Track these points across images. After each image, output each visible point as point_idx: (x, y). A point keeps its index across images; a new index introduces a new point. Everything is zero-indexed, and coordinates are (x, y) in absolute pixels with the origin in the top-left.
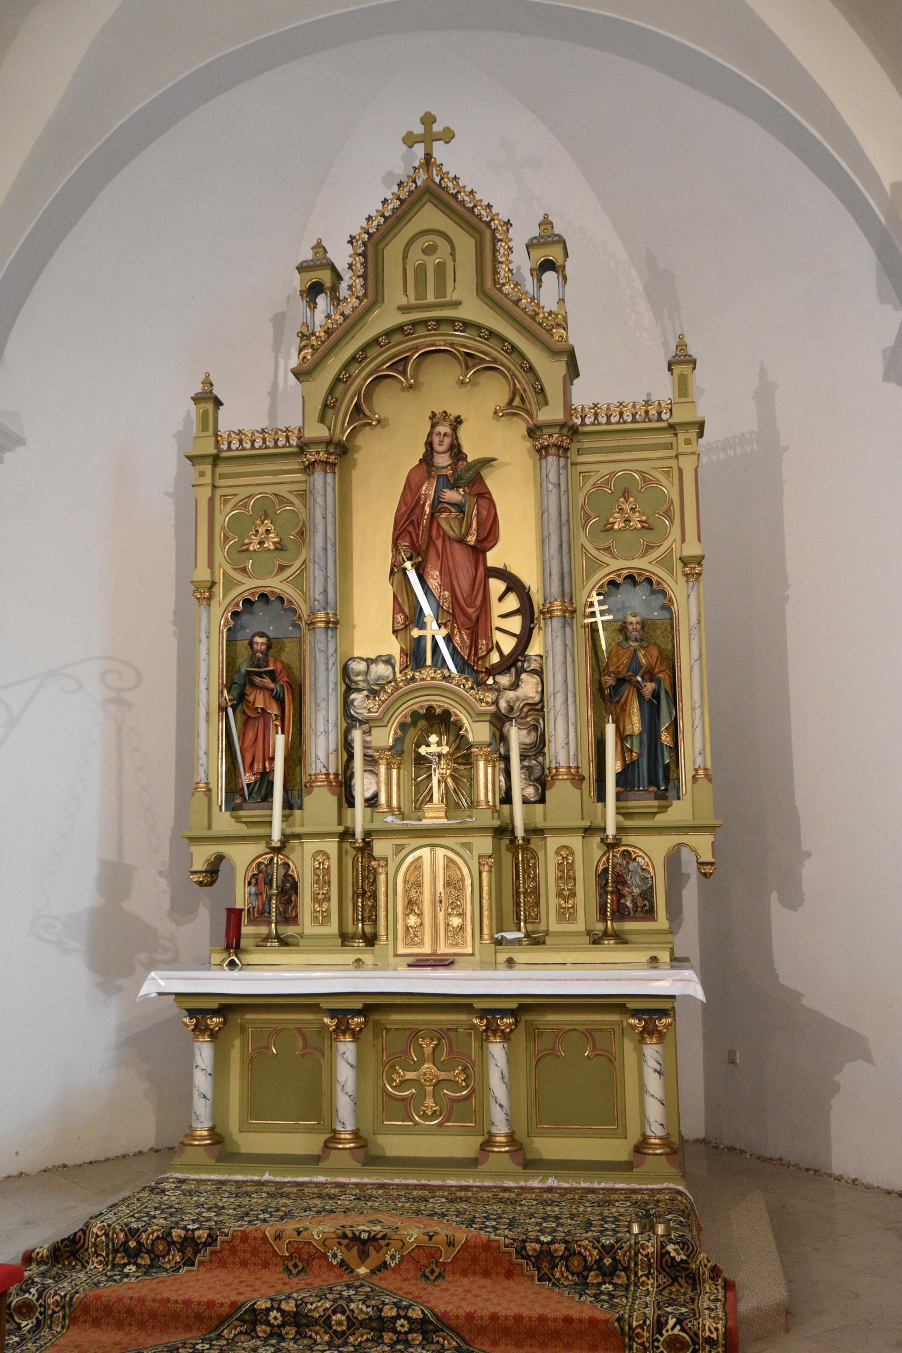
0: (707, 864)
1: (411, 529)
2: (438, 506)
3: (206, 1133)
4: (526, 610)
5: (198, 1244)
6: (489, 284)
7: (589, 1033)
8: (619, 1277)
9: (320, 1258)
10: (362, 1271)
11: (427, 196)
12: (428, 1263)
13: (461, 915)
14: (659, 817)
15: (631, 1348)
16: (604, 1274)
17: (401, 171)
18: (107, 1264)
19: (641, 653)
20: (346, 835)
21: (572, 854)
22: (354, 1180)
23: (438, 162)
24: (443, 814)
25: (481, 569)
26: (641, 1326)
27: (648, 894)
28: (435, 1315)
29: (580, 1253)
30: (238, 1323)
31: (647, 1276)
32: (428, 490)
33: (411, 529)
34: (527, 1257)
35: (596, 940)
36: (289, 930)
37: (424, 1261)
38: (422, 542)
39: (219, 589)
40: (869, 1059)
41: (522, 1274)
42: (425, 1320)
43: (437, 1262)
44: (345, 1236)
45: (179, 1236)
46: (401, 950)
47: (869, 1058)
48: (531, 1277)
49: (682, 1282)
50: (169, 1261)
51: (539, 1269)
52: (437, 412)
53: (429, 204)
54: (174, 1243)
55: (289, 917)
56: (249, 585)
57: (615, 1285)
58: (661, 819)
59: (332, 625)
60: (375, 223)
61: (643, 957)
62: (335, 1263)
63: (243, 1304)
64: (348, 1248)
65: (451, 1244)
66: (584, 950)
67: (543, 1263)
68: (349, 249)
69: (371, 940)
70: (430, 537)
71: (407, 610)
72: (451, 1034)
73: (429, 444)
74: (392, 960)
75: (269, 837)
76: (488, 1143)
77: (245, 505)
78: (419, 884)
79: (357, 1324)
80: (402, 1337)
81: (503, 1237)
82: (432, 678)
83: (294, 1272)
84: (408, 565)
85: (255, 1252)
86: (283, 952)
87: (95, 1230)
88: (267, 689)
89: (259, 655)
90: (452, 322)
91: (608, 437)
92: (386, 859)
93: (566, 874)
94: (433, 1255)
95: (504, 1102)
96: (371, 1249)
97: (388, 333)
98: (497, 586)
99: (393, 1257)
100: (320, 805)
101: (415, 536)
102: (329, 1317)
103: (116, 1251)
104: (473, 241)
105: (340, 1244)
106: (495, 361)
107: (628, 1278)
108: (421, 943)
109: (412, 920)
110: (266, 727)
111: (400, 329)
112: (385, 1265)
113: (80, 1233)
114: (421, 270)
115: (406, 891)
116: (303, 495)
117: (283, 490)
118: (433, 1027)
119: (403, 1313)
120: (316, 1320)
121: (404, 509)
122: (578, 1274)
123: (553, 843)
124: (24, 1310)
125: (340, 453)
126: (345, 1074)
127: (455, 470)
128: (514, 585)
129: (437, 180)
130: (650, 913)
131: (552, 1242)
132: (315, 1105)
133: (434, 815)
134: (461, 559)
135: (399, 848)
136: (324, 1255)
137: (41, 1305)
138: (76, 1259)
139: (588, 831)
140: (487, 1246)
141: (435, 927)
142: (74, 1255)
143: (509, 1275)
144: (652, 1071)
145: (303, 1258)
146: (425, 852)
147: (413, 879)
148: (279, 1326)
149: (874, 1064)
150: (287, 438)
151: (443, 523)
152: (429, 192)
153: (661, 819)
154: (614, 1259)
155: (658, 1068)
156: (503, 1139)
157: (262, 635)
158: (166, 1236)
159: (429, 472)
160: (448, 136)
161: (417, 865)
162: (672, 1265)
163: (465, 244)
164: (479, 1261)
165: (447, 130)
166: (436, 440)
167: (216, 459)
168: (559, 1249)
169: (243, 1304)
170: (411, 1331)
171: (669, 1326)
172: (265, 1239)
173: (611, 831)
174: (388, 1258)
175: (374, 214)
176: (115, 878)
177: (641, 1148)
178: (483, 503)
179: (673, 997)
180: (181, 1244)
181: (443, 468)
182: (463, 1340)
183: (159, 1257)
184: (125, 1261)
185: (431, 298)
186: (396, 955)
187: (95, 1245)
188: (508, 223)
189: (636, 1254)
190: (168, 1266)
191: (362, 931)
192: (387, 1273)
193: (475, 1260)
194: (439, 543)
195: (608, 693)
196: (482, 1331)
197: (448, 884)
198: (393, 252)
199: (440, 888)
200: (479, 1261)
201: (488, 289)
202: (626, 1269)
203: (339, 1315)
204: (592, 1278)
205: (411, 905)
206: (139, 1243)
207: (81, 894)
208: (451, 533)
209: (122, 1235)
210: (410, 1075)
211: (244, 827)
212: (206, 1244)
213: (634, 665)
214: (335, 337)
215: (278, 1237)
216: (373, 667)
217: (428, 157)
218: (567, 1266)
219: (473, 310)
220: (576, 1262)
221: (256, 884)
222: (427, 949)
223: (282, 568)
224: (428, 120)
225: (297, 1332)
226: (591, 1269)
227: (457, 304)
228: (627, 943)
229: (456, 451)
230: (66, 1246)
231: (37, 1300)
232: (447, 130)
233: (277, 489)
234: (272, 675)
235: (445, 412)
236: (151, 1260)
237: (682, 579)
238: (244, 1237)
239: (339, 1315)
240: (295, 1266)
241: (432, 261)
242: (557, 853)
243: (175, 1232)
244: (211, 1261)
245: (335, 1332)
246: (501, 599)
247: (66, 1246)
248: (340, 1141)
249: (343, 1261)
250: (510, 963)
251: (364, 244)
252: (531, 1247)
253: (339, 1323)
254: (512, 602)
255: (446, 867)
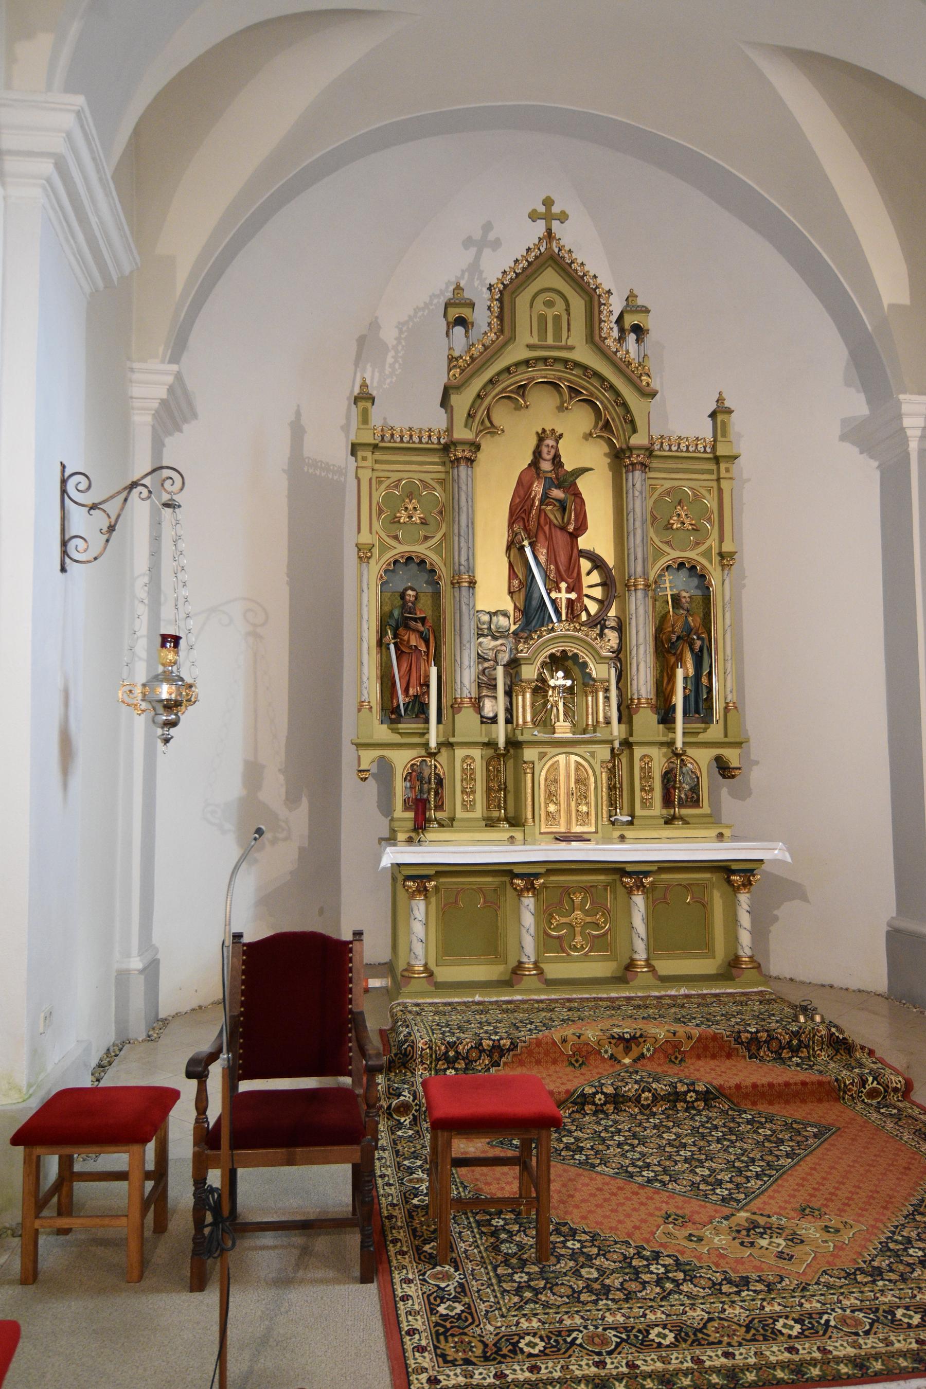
0: (364, 771)
1: (523, 515)
2: (545, 496)
3: (422, 969)
4: (607, 583)
5: (502, 1050)
6: (597, 338)
7: (688, 887)
8: (802, 1052)
9: (595, 1054)
10: (627, 1061)
11: (550, 262)
12: (672, 1052)
13: (587, 804)
14: (701, 736)
15: (844, 1099)
16: (792, 1051)
17: (532, 241)
18: (430, 1070)
19: (690, 619)
20: (491, 744)
21: (652, 760)
22: (429, 1000)
23: (557, 237)
24: (568, 730)
25: (575, 551)
26: (852, 1084)
27: (695, 789)
28: (714, 1087)
29: (777, 1038)
30: (571, 1105)
31: (820, 1050)
32: (538, 489)
33: (523, 515)
34: (742, 1043)
35: (669, 821)
36: (440, 815)
37: (670, 1051)
38: (532, 525)
39: (376, 551)
40: (804, 898)
41: (738, 1055)
42: (708, 1092)
43: (680, 1050)
44: (613, 1037)
45: (488, 1045)
46: (543, 830)
47: (804, 898)
48: (744, 1057)
49: (842, 1052)
50: (480, 1064)
51: (749, 1051)
52: (547, 429)
53: (550, 268)
54: (484, 1050)
55: (439, 807)
56: (401, 549)
57: (800, 1058)
58: (702, 737)
59: (472, 584)
60: (509, 277)
61: (713, 833)
62: (606, 1057)
63: (575, 1091)
64: (616, 1045)
65: (689, 1037)
66: (480, 831)
67: (753, 1046)
68: (487, 295)
69: (515, 822)
70: (539, 523)
71: (520, 576)
72: (593, 890)
73: (537, 454)
74: (538, 836)
75: (426, 745)
76: (630, 966)
77: (397, 487)
78: (556, 781)
79: (659, 1098)
80: (690, 1105)
81: (722, 1029)
82: (568, 630)
83: (577, 1065)
84: (526, 543)
85: (547, 1053)
86: (488, 831)
87: (420, 1045)
88: (418, 631)
89: (410, 604)
90: (565, 361)
91: (669, 461)
92: (533, 763)
93: (468, 775)
94: (677, 1046)
95: (644, 937)
96: (633, 1045)
97: (517, 364)
98: (585, 565)
99: (648, 1050)
100: (467, 724)
101: (523, 517)
102: (640, 1095)
103: (438, 1060)
104: (583, 302)
105: (610, 1043)
106: (592, 394)
107: (809, 1053)
108: (559, 824)
109: (552, 808)
110: (418, 659)
111: (527, 363)
112: (642, 1056)
113: (409, 1048)
114: (542, 319)
115: (547, 786)
116: (442, 482)
117: (427, 477)
118: (581, 885)
119: (692, 1088)
120: (630, 1098)
121: (518, 500)
122: (776, 1052)
123: (460, 753)
124: (402, 1109)
125: (455, 455)
126: (528, 920)
127: (557, 474)
128: (598, 563)
129: (556, 250)
130: (695, 802)
131: (758, 1032)
132: (492, 945)
133: (563, 730)
134: (560, 539)
135: (542, 756)
136: (599, 1052)
137: (416, 1105)
138: (406, 1068)
139: (662, 744)
140: (715, 1037)
141: (569, 812)
142: (404, 1065)
143: (729, 1056)
144: (745, 911)
145: (582, 1055)
146: (562, 759)
147: (552, 778)
148: (601, 1105)
149: (808, 902)
150: (430, 437)
151: (545, 513)
152: (550, 259)
153: (702, 737)
154: (799, 1040)
155: (748, 909)
156: (643, 963)
157: (413, 590)
158: (478, 1047)
159: (538, 474)
160: (563, 217)
161: (555, 767)
162: (837, 1042)
163: (578, 305)
164: (711, 1048)
165: (563, 212)
166: (545, 450)
167: (375, 447)
168: (764, 1036)
169: (575, 1091)
170: (697, 1100)
171: (870, 1082)
172: (554, 1043)
173: (679, 744)
174: (645, 1050)
175: (508, 269)
176: (253, 774)
177: (734, 963)
178: (578, 500)
179: (762, 860)
180: (490, 1051)
181: (547, 472)
182: (733, 1103)
183: (471, 1062)
184: (446, 1066)
185: (550, 341)
186: (541, 833)
187: (421, 1056)
188: (609, 292)
189: (814, 1036)
190: (480, 1068)
191: (508, 813)
192: (645, 1061)
193: (706, 1048)
194: (547, 528)
195: (666, 650)
196: (746, 1096)
197: (577, 781)
198: (523, 300)
199: (572, 785)
200: (711, 1048)
201: (593, 339)
202: (807, 1047)
203: (647, 1093)
204: (785, 1054)
205: (551, 797)
206: (457, 1052)
207: (231, 788)
208: (555, 522)
209: (443, 1047)
210: (564, 920)
211: (398, 736)
212: (509, 1050)
213: (689, 630)
214: (476, 364)
215: (564, 1041)
216: (494, 619)
217: (549, 231)
218: (768, 1048)
219: (583, 354)
220: (774, 1044)
221: (410, 781)
222: (563, 829)
223: (426, 538)
224: (548, 202)
225: (615, 1108)
226: (784, 1048)
227: (571, 348)
228: (688, 823)
229: (557, 461)
230: (400, 1058)
231: (413, 1101)
232: (563, 212)
233: (423, 476)
234: (423, 620)
235: (553, 430)
236: (466, 1064)
237: (719, 568)
238: (539, 1043)
239: (647, 1093)
240: (577, 1061)
241: (550, 313)
242: (463, 761)
243: (484, 1043)
244: (513, 1062)
245: (643, 1105)
246: (588, 574)
247: (400, 1058)
248: (524, 969)
249: (612, 1055)
250: (622, 838)
251: (501, 292)
252: (745, 1036)
253: (647, 1099)
254: (595, 577)
255: (577, 769)
